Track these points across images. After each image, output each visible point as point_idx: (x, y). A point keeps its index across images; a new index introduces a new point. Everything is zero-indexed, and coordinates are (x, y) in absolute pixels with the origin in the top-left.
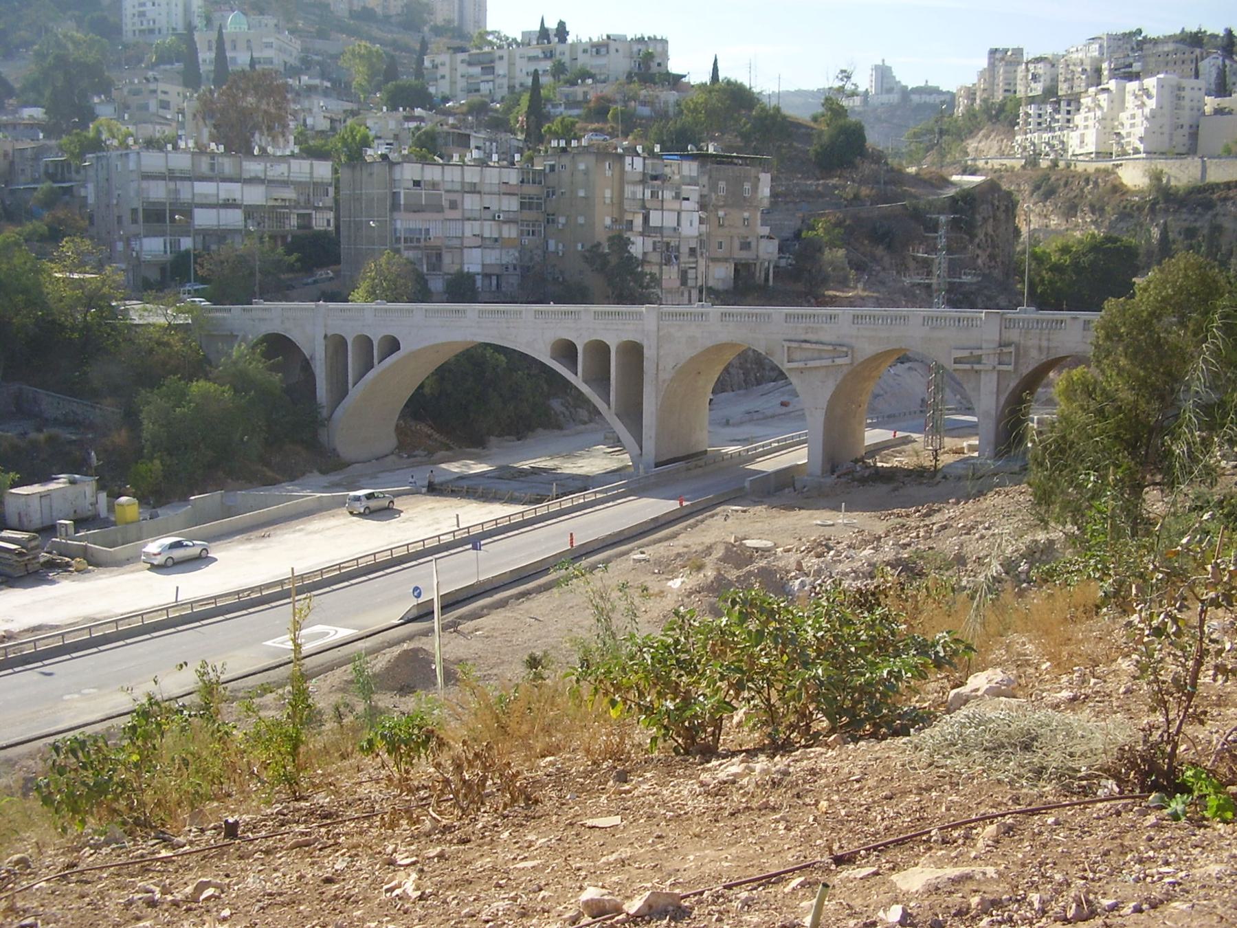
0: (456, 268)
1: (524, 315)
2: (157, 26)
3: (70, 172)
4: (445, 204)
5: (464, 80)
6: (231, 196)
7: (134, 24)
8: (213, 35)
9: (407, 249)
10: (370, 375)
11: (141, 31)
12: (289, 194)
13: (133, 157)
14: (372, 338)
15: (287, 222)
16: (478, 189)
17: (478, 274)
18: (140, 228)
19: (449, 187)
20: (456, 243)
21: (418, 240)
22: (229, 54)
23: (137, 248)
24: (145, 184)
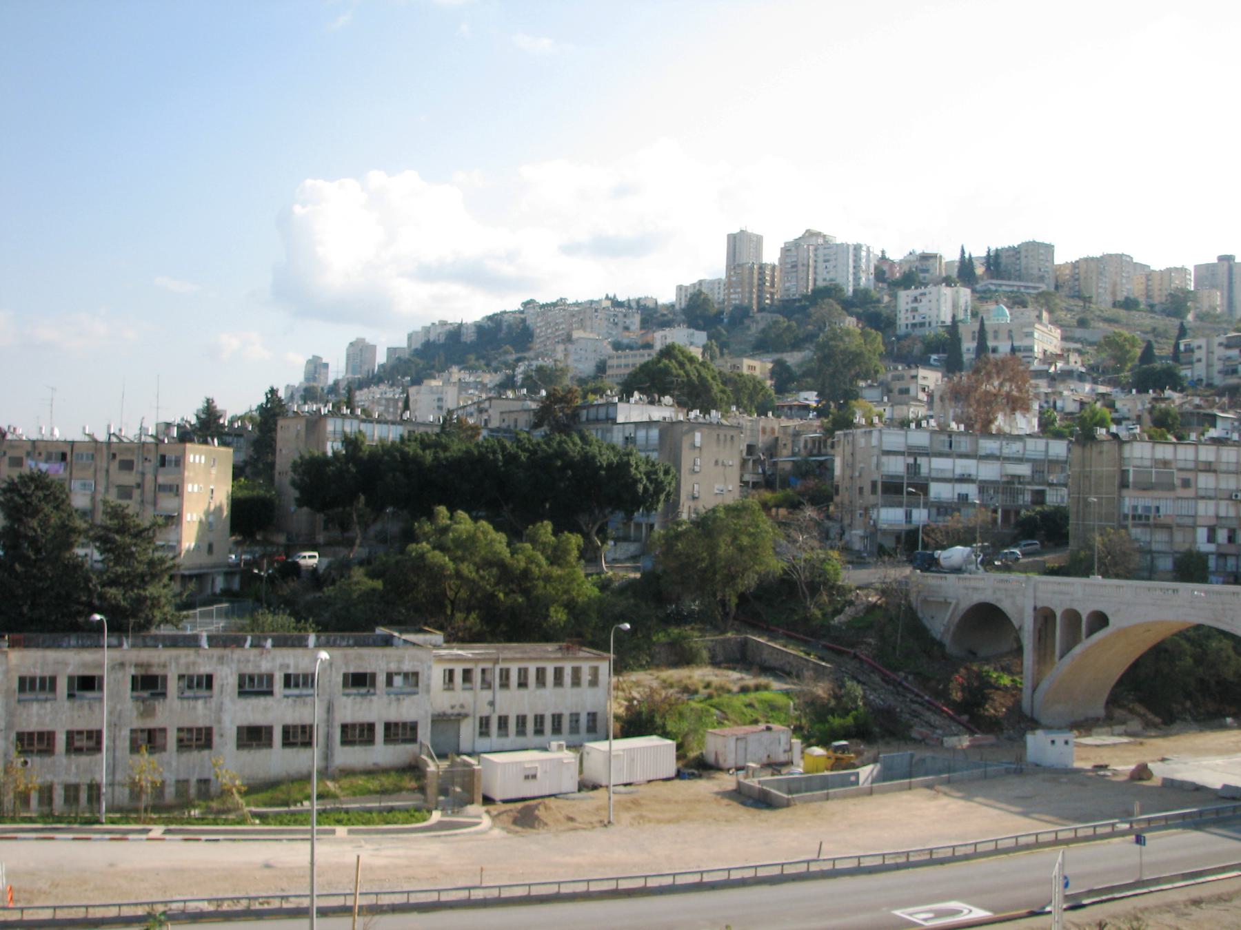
0: (1187, 546)
1: (1180, 592)
2: (927, 320)
3: (825, 447)
4: (1177, 482)
5: (1221, 362)
6: (967, 472)
7: (907, 318)
8: (976, 327)
9: (1135, 526)
10: (1077, 650)
11: (914, 325)
12: (1024, 470)
13: (875, 434)
14: (1080, 611)
15: (1021, 497)
16: (1213, 467)
17: (1212, 553)
18: (879, 498)
19: (1181, 465)
20: (1189, 521)
21: (1147, 518)
22: (991, 344)
23: (874, 516)
24: (884, 459)
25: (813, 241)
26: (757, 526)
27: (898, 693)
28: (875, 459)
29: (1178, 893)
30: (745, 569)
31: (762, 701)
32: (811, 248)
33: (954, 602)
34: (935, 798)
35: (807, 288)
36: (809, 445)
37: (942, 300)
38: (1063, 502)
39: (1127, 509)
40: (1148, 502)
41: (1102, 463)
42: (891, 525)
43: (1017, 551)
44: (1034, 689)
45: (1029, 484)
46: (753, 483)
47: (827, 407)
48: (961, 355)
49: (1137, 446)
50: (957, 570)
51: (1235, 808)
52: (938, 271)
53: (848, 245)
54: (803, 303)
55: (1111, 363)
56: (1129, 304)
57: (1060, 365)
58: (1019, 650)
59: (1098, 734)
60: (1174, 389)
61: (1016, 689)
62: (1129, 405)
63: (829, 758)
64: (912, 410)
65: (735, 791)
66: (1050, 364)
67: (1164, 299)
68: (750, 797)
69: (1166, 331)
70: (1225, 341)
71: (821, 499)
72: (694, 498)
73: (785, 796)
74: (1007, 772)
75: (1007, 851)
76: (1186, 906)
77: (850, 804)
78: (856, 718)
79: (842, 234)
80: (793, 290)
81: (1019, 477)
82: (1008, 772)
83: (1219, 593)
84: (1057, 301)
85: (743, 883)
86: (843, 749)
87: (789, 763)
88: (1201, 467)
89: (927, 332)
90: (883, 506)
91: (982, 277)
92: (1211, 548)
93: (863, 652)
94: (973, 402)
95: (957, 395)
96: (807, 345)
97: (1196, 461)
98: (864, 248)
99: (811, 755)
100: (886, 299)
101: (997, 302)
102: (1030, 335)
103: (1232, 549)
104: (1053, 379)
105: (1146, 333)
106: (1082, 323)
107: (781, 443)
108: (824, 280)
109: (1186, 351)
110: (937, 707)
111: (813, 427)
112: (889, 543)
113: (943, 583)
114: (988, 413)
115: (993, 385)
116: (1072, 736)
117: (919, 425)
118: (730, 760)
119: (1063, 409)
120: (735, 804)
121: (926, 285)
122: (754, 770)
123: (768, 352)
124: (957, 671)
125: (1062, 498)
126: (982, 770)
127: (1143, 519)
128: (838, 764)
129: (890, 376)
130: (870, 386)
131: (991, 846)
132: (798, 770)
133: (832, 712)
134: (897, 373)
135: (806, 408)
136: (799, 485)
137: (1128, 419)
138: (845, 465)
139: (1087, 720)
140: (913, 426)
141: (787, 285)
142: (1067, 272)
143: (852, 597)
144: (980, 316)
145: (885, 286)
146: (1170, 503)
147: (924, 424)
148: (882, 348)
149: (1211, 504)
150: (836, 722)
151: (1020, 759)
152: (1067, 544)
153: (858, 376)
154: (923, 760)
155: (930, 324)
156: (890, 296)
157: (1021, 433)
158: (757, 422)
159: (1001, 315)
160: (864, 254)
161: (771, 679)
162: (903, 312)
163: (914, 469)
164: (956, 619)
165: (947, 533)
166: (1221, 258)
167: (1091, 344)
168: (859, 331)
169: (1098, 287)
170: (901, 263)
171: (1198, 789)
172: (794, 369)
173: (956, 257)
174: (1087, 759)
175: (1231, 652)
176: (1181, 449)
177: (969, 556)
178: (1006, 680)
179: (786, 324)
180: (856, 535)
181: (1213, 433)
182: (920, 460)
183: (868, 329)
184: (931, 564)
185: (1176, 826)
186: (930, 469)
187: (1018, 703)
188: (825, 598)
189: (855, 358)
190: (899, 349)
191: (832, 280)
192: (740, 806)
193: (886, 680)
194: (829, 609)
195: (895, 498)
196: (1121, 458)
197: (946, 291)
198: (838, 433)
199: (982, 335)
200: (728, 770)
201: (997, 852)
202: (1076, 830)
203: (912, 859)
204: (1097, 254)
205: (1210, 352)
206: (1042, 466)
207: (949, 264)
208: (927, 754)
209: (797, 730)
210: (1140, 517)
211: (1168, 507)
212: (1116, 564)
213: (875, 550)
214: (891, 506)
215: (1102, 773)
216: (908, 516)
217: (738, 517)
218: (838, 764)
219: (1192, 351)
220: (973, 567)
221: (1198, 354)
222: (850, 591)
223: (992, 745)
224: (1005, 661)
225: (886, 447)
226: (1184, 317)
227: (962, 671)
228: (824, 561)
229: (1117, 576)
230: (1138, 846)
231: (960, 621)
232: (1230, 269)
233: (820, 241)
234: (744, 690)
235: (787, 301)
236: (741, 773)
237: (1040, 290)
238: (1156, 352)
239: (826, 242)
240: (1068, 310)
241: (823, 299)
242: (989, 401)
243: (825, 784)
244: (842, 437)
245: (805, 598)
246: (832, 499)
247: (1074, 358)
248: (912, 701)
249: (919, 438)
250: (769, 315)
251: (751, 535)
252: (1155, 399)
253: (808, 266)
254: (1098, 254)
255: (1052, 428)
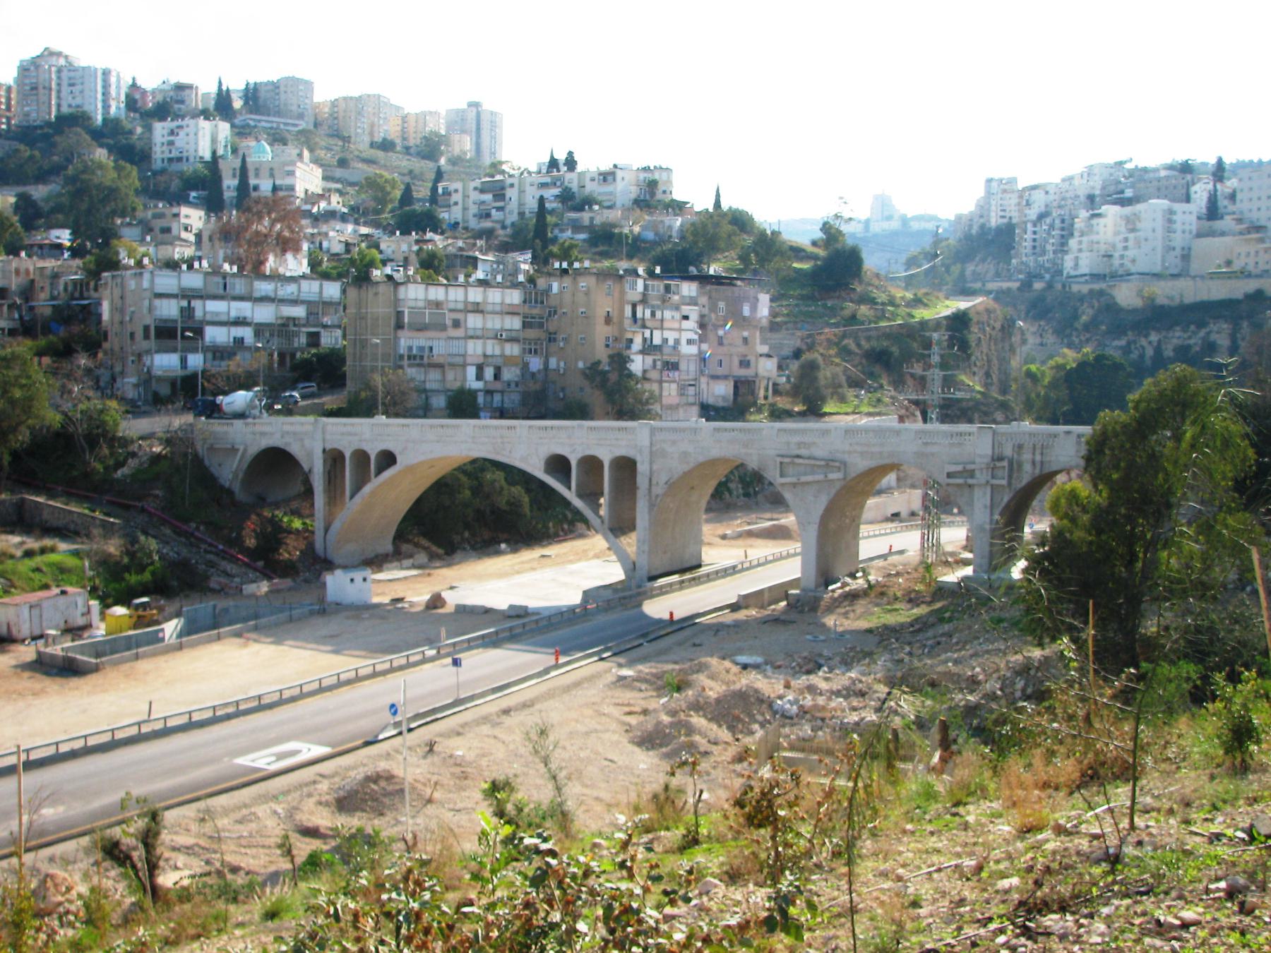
2: (185, 154)
3: (88, 290)
4: (449, 322)
6: (242, 315)
8: (237, 163)
9: (410, 366)
10: (367, 489)
11: (170, 160)
12: (299, 312)
13: (147, 276)
14: (369, 452)
18: (152, 343)
19: (452, 306)
20: (459, 360)
21: (422, 357)
22: (252, 181)
23: (148, 363)
24: (157, 302)
25: (54, 60)
26: (29, 377)
27: (191, 545)
28: (146, 303)
29: (491, 706)
30: (19, 424)
31: (50, 565)
32: (54, 69)
33: (242, 448)
34: (245, 645)
35: (50, 114)
36: (70, 288)
37: (201, 133)
38: (337, 343)
39: (402, 350)
40: (422, 343)
41: (378, 306)
43: (296, 394)
44: (327, 530)
45: (304, 326)
46: (9, 330)
47: (82, 246)
48: (221, 193)
49: (411, 287)
50: (241, 415)
51: (524, 625)
52: (195, 101)
53: (96, 69)
54: (46, 130)
55: (372, 204)
56: (387, 145)
57: (323, 205)
58: (309, 492)
59: (389, 569)
60: (435, 231)
61: (307, 533)
62: (393, 247)
63: (131, 617)
64: (177, 250)
65: (36, 662)
66: (313, 204)
67: (418, 142)
68: (52, 666)
69: (422, 174)
70: (479, 186)
71: (93, 344)
73: (93, 661)
74: (312, 613)
75: (330, 688)
76: (498, 716)
77: (161, 661)
78: (153, 573)
79: (85, 55)
80: (34, 115)
81: (294, 319)
82: (312, 613)
83: (487, 427)
84: (317, 139)
85: (73, 755)
86: (144, 606)
87: (89, 626)
88: (470, 308)
89: (186, 168)
90: (157, 352)
91: (240, 112)
92: (478, 385)
93: (151, 505)
94: (243, 242)
95: (227, 235)
96: (52, 178)
97: (466, 302)
98: (114, 74)
99: (112, 616)
100: (139, 130)
101: (258, 140)
102: (291, 173)
103: (498, 386)
104: (317, 219)
105: (404, 175)
106: (343, 163)
107: (38, 286)
108: (70, 106)
109: (444, 194)
110: (232, 556)
111: (73, 269)
112: (165, 390)
113: (230, 429)
114: (259, 255)
115: (263, 226)
116: (367, 573)
117: (190, 267)
118: (25, 630)
119: (328, 251)
120: (38, 675)
121: (183, 118)
122: (54, 637)
123: (7, 184)
124: (248, 518)
125: (336, 339)
126: (287, 613)
127: (418, 359)
128: (140, 622)
129: (150, 214)
130: (129, 224)
131: (316, 686)
132: (100, 631)
133: (127, 569)
134: (157, 211)
135: (59, 247)
136: (62, 332)
137: (392, 260)
138: (113, 309)
139: (377, 556)
140: (184, 267)
141: (26, 109)
142: (326, 110)
143: (134, 448)
144: (241, 153)
145: (137, 115)
146: (442, 343)
147: (196, 265)
148: (137, 184)
149: (479, 342)
150: (133, 579)
151: (322, 599)
152: (343, 385)
153: (114, 213)
154: (226, 610)
155: (187, 159)
156: (143, 127)
157: (295, 274)
158: (10, 262)
159: (262, 152)
160: (113, 80)
161: (57, 540)
162: (159, 145)
163: (188, 312)
164: (245, 465)
165: (228, 378)
166: (471, 105)
167: (352, 184)
168: (112, 164)
169: (356, 127)
170: (154, 92)
171: (487, 611)
172: (42, 204)
173: (213, 89)
174: (383, 594)
175: (503, 483)
176: (452, 290)
177: (252, 400)
178: (297, 524)
179: (28, 154)
180: (129, 384)
181: (480, 274)
182: (193, 303)
183: (122, 163)
184: (213, 410)
185: (477, 647)
186: (205, 313)
187: (311, 546)
188: (106, 451)
189: (111, 193)
190: (155, 185)
191: (78, 106)
192: (44, 677)
193: (179, 532)
194: (111, 462)
195: (170, 343)
196: (397, 301)
197: (203, 123)
198: (105, 274)
199: (243, 172)
200: (23, 641)
201: (321, 690)
202: (391, 661)
203: (241, 707)
204: (355, 93)
205: (466, 196)
206: (317, 307)
207: (206, 95)
208: (228, 603)
209: (93, 592)
210: (415, 357)
211: (441, 347)
212: (395, 404)
213: (150, 398)
215: (400, 605)
216: (184, 361)
217: (8, 367)
218: (140, 622)
219: (450, 194)
220: (256, 412)
221: (456, 197)
222: (132, 442)
223: (290, 589)
224: (294, 505)
225: (159, 290)
226: (437, 161)
227: (254, 517)
228: (102, 411)
229: (397, 415)
230: (454, 669)
231: (250, 466)
232: (478, 115)
233: (62, 62)
234: (29, 554)
235: (28, 127)
236: (41, 642)
237: (300, 128)
238: (415, 195)
239: (70, 64)
240: (329, 149)
241: (70, 127)
242: (259, 241)
243: (130, 644)
244: (110, 280)
245: (84, 452)
246: (100, 346)
247: (335, 199)
248: (206, 551)
249: (193, 281)
250: (7, 143)
251: (22, 387)
252: (417, 242)
253: (50, 89)
254: (356, 94)
255: (319, 269)
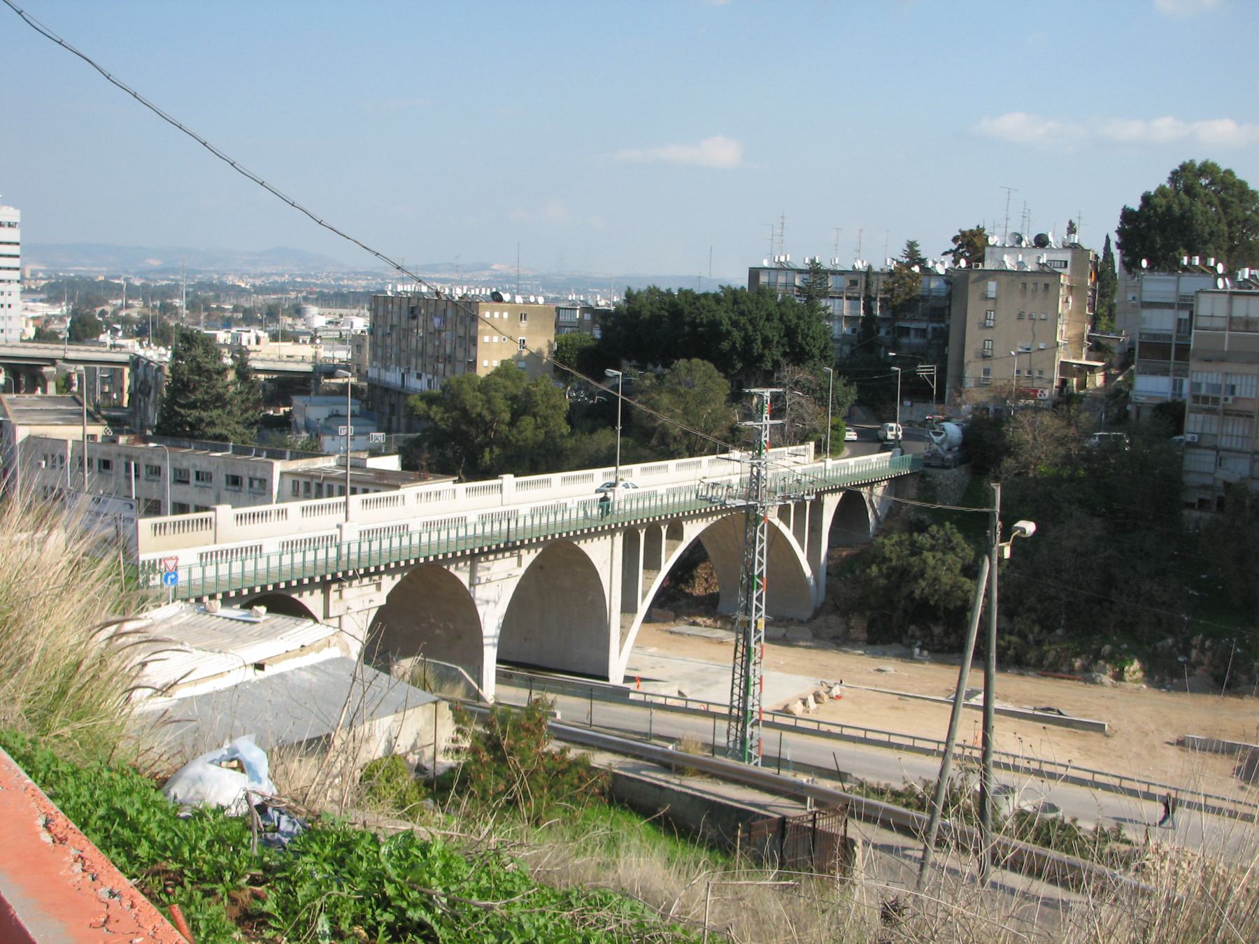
21: (1216, 400)
42: (1149, 397)
72: (985, 357)
210: (1205, 399)
214: (1154, 373)
